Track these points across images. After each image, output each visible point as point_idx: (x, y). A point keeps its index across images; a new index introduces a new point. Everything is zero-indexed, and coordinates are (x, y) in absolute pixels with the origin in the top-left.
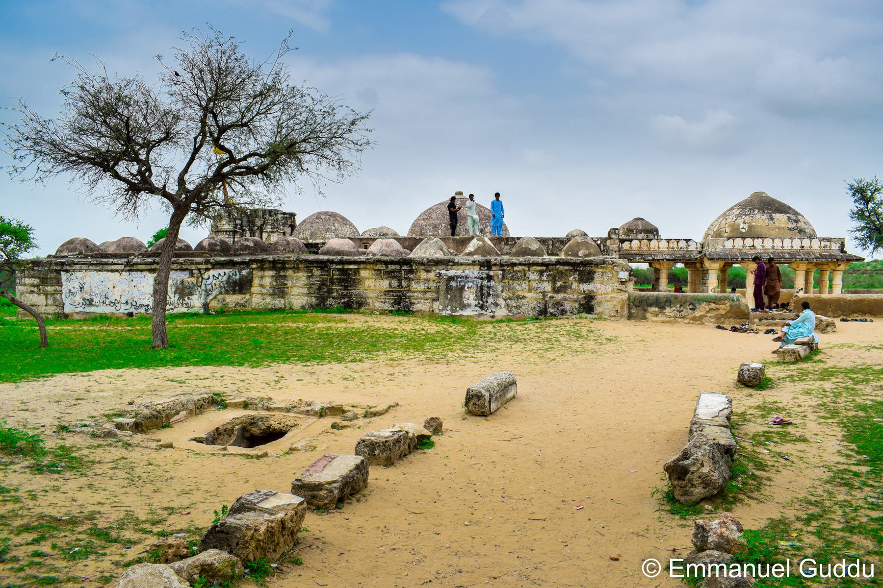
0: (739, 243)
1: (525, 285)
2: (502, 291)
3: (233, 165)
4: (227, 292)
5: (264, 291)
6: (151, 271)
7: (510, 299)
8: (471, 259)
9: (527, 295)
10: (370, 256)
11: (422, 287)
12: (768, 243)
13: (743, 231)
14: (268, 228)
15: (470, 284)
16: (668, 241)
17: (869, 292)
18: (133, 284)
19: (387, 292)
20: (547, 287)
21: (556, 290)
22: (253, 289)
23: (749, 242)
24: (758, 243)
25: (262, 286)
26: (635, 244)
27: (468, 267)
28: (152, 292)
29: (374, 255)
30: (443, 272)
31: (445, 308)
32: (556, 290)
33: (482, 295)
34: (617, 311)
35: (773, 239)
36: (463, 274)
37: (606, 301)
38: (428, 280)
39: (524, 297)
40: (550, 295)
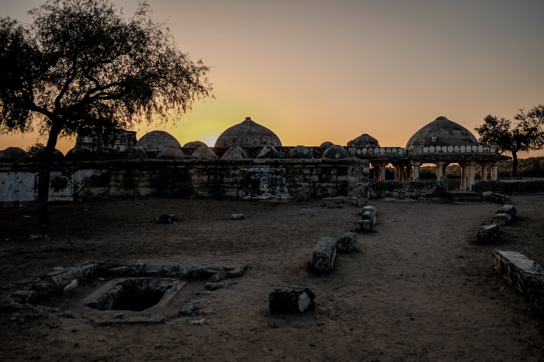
0: (432, 149)
1: (301, 177)
2: (286, 182)
3: (99, 92)
4: (91, 186)
5: (119, 184)
6: (33, 171)
7: (292, 187)
8: (264, 161)
9: (303, 184)
10: (194, 160)
11: (231, 180)
12: (451, 149)
13: (434, 141)
14: (118, 142)
15: (264, 178)
16: (386, 148)
17: (521, 179)
18: (19, 180)
19: (206, 184)
20: (316, 178)
21: (321, 181)
22: (111, 183)
23: (438, 148)
24: (444, 149)
25: (118, 181)
26: (365, 150)
27: (262, 166)
28: (33, 187)
29: (197, 158)
30: (245, 169)
31: (247, 194)
32: (321, 181)
33: (272, 184)
34: (362, 194)
35: (454, 147)
36: (260, 171)
37: (356, 187)
38: (235, 175)
39: (301, 186)
40: (318, 184)
